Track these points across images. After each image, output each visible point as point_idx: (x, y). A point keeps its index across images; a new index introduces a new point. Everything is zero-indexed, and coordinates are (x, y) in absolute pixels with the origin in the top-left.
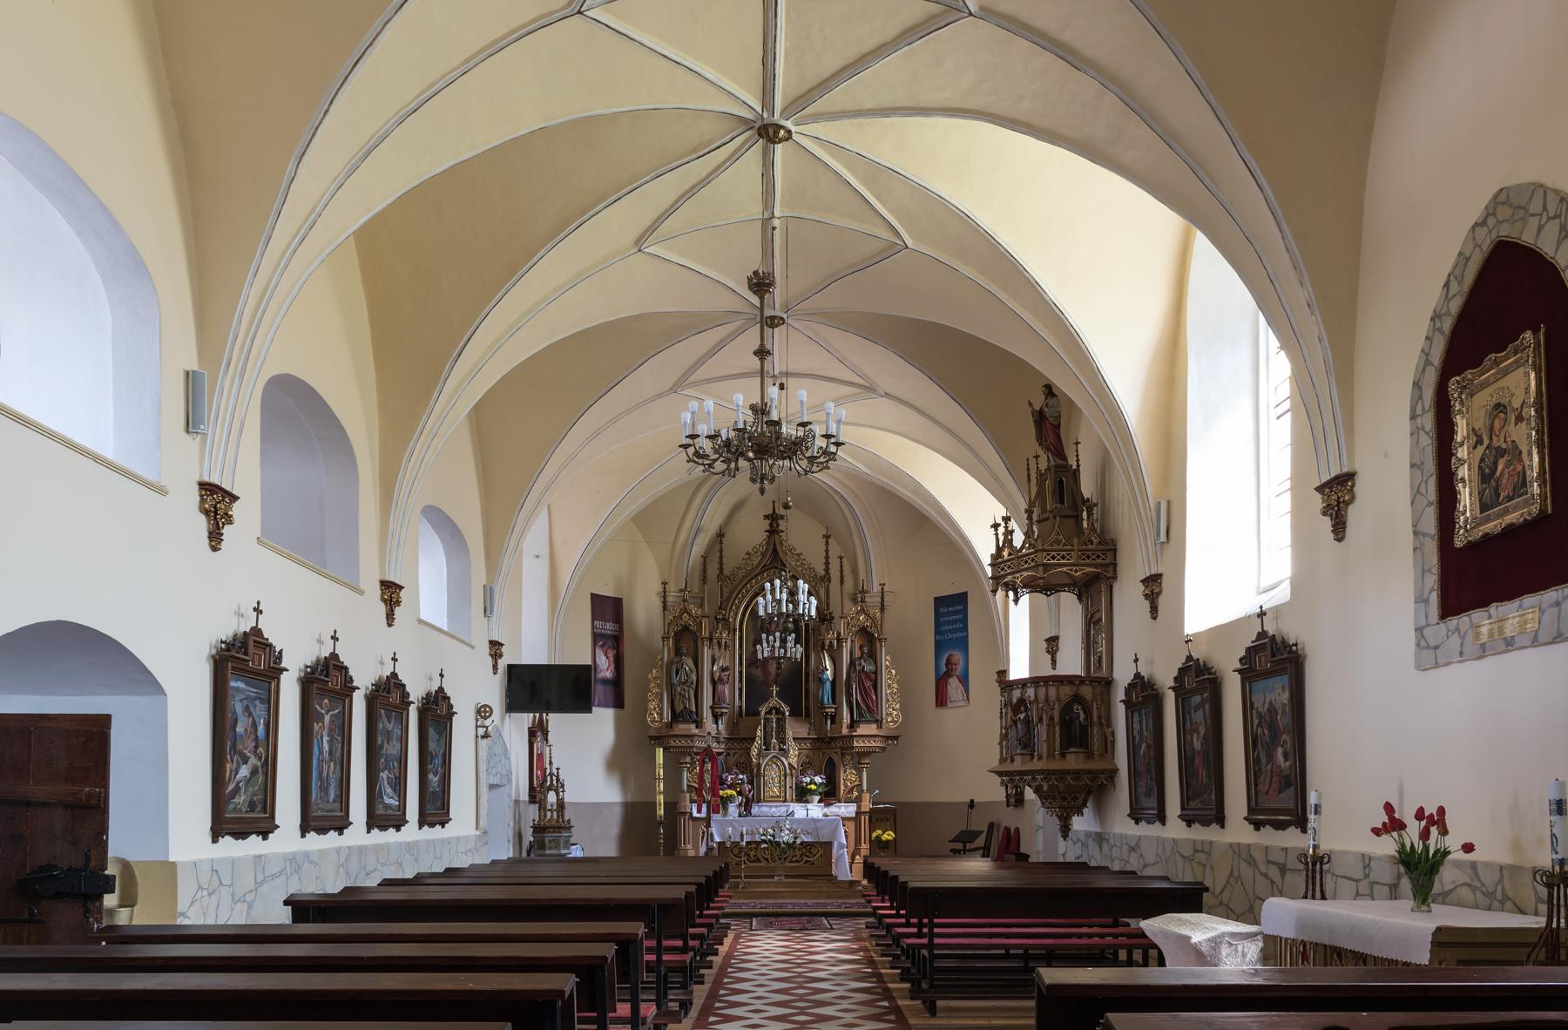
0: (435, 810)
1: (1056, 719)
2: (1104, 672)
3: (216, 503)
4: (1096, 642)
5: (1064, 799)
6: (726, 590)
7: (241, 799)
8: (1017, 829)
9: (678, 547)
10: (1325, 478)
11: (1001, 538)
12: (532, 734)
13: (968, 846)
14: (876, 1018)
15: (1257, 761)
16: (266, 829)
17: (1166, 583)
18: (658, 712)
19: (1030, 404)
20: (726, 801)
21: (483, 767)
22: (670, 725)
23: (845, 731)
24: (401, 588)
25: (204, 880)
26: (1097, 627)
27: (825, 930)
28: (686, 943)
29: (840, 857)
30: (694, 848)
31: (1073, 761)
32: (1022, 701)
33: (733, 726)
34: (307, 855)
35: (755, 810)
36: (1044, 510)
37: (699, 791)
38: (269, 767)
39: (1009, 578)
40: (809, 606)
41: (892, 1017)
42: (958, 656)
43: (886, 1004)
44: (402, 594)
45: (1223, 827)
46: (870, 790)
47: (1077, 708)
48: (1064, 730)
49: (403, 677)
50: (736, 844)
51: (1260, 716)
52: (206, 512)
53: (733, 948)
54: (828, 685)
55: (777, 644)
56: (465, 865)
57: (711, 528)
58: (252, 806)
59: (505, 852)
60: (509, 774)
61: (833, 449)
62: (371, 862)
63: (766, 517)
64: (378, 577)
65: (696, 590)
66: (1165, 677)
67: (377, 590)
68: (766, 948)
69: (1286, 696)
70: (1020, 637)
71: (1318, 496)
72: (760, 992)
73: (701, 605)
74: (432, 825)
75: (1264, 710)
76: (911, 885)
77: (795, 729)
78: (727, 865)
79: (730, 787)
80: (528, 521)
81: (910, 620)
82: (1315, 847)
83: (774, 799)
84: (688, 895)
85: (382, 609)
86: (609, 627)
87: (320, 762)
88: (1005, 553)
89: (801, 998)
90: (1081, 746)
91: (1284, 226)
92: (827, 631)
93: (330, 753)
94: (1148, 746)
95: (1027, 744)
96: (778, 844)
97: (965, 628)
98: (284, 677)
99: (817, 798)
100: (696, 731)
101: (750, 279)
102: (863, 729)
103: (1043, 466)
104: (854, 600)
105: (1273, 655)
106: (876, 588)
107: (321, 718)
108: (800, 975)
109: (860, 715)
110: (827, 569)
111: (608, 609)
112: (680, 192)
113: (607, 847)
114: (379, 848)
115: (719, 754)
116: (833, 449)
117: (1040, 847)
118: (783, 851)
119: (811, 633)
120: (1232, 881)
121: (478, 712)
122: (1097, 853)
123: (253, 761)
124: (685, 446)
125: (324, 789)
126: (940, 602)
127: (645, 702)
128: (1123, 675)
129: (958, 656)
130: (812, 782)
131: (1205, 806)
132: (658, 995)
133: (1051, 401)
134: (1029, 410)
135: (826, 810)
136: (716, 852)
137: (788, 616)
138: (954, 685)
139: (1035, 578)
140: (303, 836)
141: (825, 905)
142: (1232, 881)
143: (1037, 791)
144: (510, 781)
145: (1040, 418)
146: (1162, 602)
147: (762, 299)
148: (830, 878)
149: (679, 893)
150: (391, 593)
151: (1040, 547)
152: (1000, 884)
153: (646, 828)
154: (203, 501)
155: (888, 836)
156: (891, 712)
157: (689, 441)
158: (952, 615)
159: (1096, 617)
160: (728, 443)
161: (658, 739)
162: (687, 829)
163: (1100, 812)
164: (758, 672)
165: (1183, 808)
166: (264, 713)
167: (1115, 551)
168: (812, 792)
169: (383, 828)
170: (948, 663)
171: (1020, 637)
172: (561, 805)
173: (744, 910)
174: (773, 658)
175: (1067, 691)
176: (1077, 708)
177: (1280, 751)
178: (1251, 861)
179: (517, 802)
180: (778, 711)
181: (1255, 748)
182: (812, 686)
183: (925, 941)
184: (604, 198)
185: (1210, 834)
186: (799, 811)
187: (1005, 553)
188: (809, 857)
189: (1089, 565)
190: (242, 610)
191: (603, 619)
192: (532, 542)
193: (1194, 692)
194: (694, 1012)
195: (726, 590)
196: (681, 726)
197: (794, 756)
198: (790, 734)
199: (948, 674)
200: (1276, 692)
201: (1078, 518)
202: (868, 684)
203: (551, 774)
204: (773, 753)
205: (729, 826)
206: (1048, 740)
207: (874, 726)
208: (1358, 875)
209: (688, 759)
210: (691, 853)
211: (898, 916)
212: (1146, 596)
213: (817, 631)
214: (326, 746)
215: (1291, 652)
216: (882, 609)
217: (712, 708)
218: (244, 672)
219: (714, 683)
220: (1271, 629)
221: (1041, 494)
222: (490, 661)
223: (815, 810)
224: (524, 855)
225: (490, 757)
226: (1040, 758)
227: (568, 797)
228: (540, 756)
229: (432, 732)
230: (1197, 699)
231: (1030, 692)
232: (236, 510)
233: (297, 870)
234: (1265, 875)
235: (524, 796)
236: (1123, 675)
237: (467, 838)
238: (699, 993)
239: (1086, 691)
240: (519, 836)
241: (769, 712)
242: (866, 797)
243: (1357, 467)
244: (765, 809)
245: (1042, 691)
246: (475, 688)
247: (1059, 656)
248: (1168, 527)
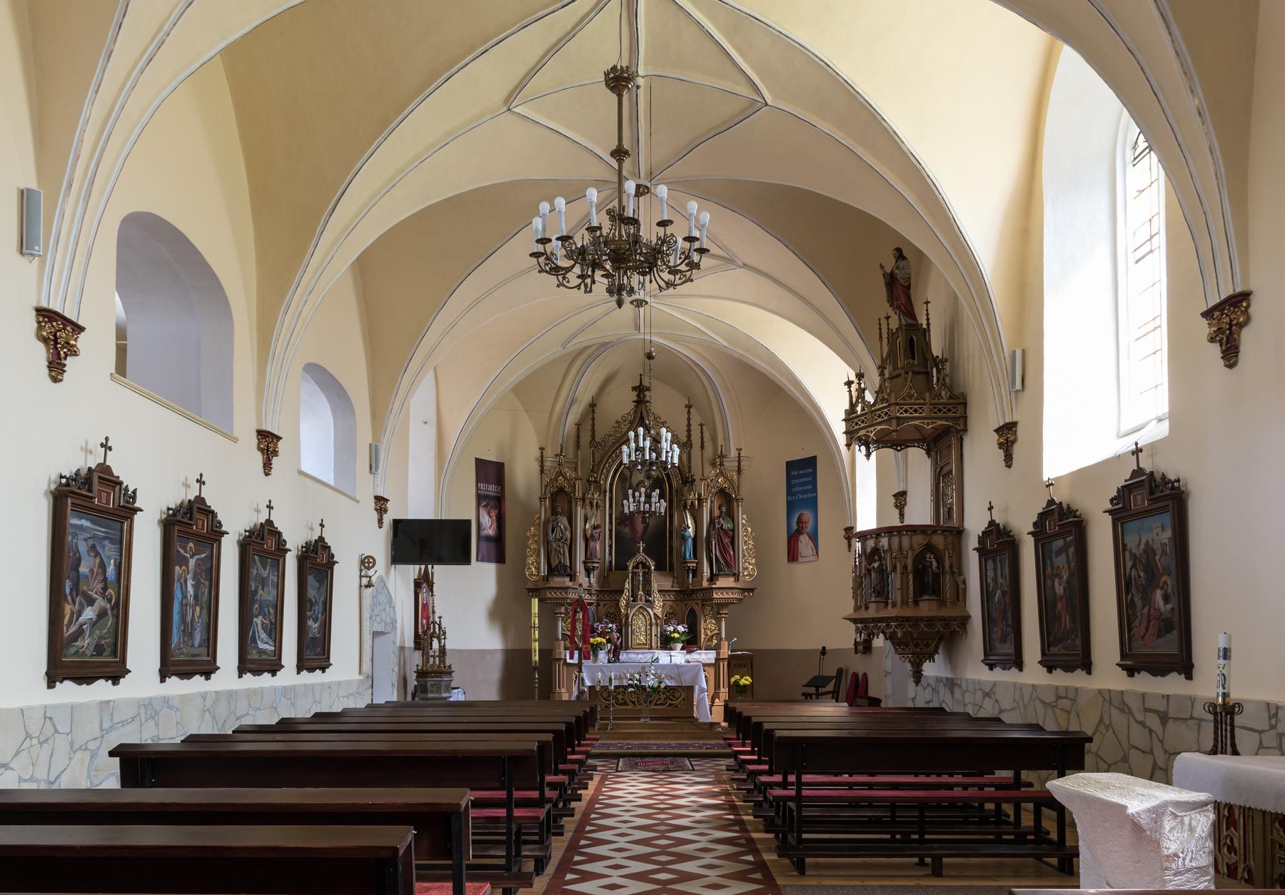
0: (315, 654)
1: (910, 568)
2: (955, 523)
3: (58, 333)
4: (945, 494)
5: (917, 645)
6: (597, 456)
7: (86, 642)
8: (865, 675)
9: (555, 416)
10: (1214, 300)
11: (855, 394)
12: (417, 585)
13: (821, 690)
14: (741, 876)
15: (1131, 604)
16: (208, 670)
17: (1021, 432)
18: (536, 567)
19: (882, 267)
20: (596, 648)
21: (366, 615)
22: (546, 579)
23: (705, 584)
24: (279, 438)
25: (34, 728)
26: (947, 480)
27: (687, 771)
28: (542, 793)
29: (701, 701)
30: (567, 693)
31: (926, 608)
32: (876, 550)
33: (603, 580)
34: (166, 700)
35: (623, 656)
36: (895, 368)
37: (572, 638)
38: (120, 609)
39: (862, 433)
40: (673, 454)
41: (758, 876)
42: (808, 515)
43: (750, 858)
44: (280, 444)
45: (1089, 672)
46: (728, 638)
47: (930, 557)
48: (915, 579)
49: (279, 524)
50: (605, 688)
51: (1134, 557)
52: (45, 340)
53: (598, 791)
54: (690, 542)
55: (643, 499)
56: (337, 708)
57: (585, 398)
58: (99, 650)
59: (388, 693)
60: (394, 622)
61: (696, 257)
62: (242, 707)
63: (634, 389)
64: (254, 427)
65: (571, 455)
66: (1022, 523)
67: (253, 440)
68: (628, 793)
69: (1168, 533)
70: (867, 491)
71: (1204, 322)
72: (622, 842)
73: (576, 470)
74: (311, 670)
75: (1138, 552)
76: (778, 734)
77: (660, 582)
78: (593, 710)
79: (599, 635)
80: (412, 384)
81: (765, 484)
82: (1225, 695)
83: (641, 647)
84: (543, 746)
85: (259, 458)
86: (492, 489)
87: (183, 606)
88: (859, 409)
89: (664, 851)
90: (934, 593)
91: (1174, 28)
92: (689, 492)
93: (196, 597)
94: (1004, 593)
95: (881, 591)
96: (644, 688)
97: (815, 490)
98: (224, 539)
99: (680, 645)
100: (570, 584)
101: (607, 74)
102: (721, 582)
103: (894, 324)
104: (713, 465)
105: (1152, 493)
106: (734, 454)
107: (184, 562)
108: (662, 822)
109: (719, 569)
110: (689, 436)
111: (491, 474)
112: (547, 46)
113: (488, 690)
114: (250, 693)
115: (590, 604)
116: (696, 257)
117: (889, 692)
118: (649, 695)
119: (673, 483)
120: (1102, 728)
121: (362, 562)
122: (948, 697)
123: (100, 603)
124: (535, 255)
125: (188, 632)
126: (791, 466)
127: (525, 557)
128: (975, 523)
129: (808, 515)
130: (675, 631)
131: (1069, 649)
132: (509, 851)
133: (901, 264)
134: (881, 273)
135: (688, 657)
136: (587, 695)
137: (651, 464)
138: (804, 542)
139: (889, 432)
140: (240, 676)
141: (687, 746)
142: (1102, 728)
143: (891, 638)
144: (395, 628)
145: (891, 281)
146: (1017, 450)
147: (620, 96)
148: (691, 719)
149: (530, 743)
150: (268, 443)
151: (893, 401)
152: (858, 733)
153: (526, 674)
154: (40, 328)
155: (746, 681)
156: (747, 566)
157: (540, 248)
158: (805, 478)
159: (946, 470)
160: (582, 252)
161: (535, 591)
162: (562, 674)
163: (952, 659)
164: (627, 530)
165: (1043, 654)
166: (115, 554)
167: (965, 404)
168: (675, 640)
169: (257, 672)
170: (799, 521)
171: (867, 491)
172: (443, 651)
173: (612, 750)
174: (639, 512)
175: (919, 540)
176: (930, 557)
177: (1159, 593)
178: (1125, 708)
179: (402, 648)
180: (645, 566)
181: (1128, 592)
182: (675, 543)
183: (793, 793)
184: (472, 49)
185: (1076, 680)
186: (664, 657)
187: (859, 409)
188: (673, 700)
190: (91, 446)
191: (487, 482)
192: (419, 402)
193: (1056, 536)
194: (550, 869)
195: (597, 456)
196: (556, 579)
197: (658, 608)
198: (655, 586)
199: (799, 532)
200: (1158, 532)
201: (928, 375)
202: (726, 540)
203: (434, 623)
204: (640, 604)
205: (599, 671)
206: (901, 588)
207: (732, 579)
208: (1264, 725)
209: (563, 610)
210: (565, 697)
211: (759, 762)
212: (1001, 445)
213: (680, 492)
214: (191, 590)
215: (1173, 488)
216: (739, 471)
217: (585, 563)
218: (86, 508)
219: (586, 540)
220: (1146, 465)
221: (892, 352)
222: (375, 515)
223: (678, 656)
224: (409, 698)
225: (375, 604)
226: (894, 605)
227: (450, 644)
228: (425, 606)
229: (311, 580)
230: (1059, 543)
231: (884, 542)
232: (82, 342)
233: (154, 716)
234: (1143, 724)
235: (410, 643)
236: (975, 523)
237: (349, 682)
238: (558, 847)
239: (938, 541)
240: (404, 681)
241: (636, 567)
242: (725, 644)
243: (1252, 286)
244: (632, 656)
245: (896, 540)
246: (358, 539)
247: (906, 510)
248: (1023, 375)
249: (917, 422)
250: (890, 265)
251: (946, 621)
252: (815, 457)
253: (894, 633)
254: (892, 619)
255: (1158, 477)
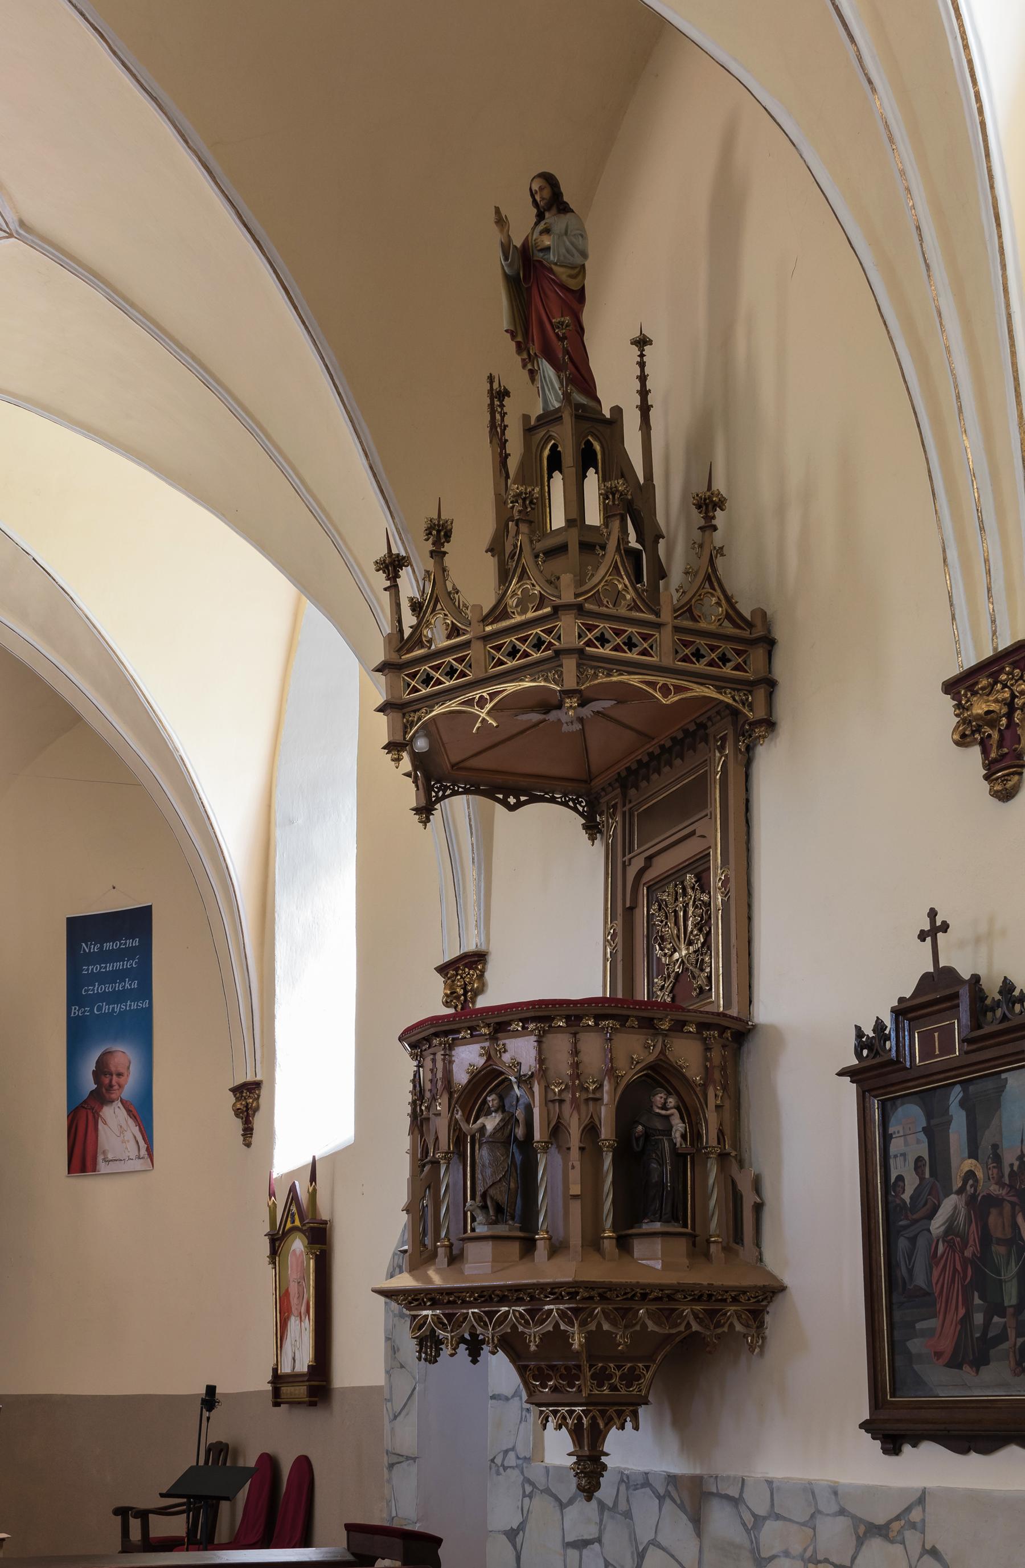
1: (607, 1132)
5: (601, 1378)
8: (304, 1465)
10: (954, 671)
19: (501, 221)
31: (653, 1261)
32: (490, 1079)
42: (125, 1055)
71: (440, 979)
95: (514, 1211)
97: (145, 991)
126: (79, 929)
129: (125, 1055)
133: (557, 222)
134: (496, 237)
138: (115, 1125)
146: (258, 1121)
165: (877, 1400)
167: (769, 643)
170: (102, 1070)
175: (634, 1049)
189: (701, 678)
199: (101, 1097)
212: (237, 1113)
226: (556, 1249)
231: (521, 1050)
249: (635, 680)
250: (522, 224)
251: (712, 1301)
252: (149, 909)
253: (557, 1339)
254: (555, 1292)
255: (992, 988)
